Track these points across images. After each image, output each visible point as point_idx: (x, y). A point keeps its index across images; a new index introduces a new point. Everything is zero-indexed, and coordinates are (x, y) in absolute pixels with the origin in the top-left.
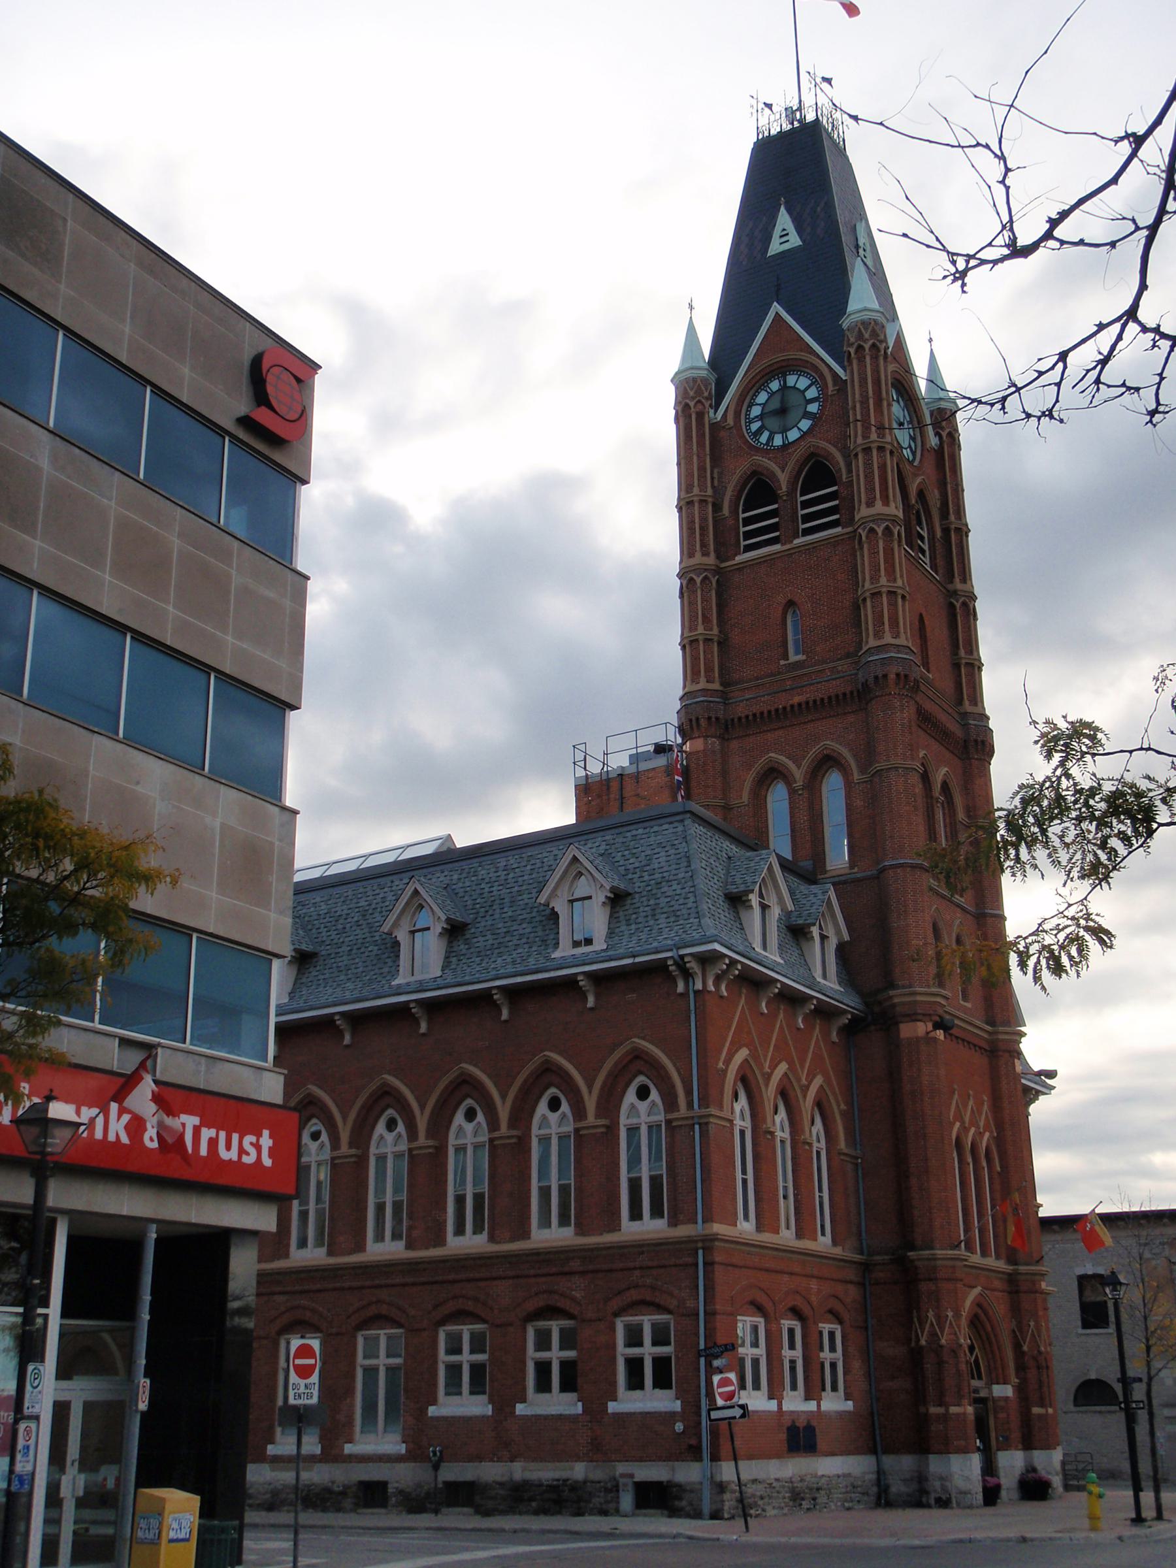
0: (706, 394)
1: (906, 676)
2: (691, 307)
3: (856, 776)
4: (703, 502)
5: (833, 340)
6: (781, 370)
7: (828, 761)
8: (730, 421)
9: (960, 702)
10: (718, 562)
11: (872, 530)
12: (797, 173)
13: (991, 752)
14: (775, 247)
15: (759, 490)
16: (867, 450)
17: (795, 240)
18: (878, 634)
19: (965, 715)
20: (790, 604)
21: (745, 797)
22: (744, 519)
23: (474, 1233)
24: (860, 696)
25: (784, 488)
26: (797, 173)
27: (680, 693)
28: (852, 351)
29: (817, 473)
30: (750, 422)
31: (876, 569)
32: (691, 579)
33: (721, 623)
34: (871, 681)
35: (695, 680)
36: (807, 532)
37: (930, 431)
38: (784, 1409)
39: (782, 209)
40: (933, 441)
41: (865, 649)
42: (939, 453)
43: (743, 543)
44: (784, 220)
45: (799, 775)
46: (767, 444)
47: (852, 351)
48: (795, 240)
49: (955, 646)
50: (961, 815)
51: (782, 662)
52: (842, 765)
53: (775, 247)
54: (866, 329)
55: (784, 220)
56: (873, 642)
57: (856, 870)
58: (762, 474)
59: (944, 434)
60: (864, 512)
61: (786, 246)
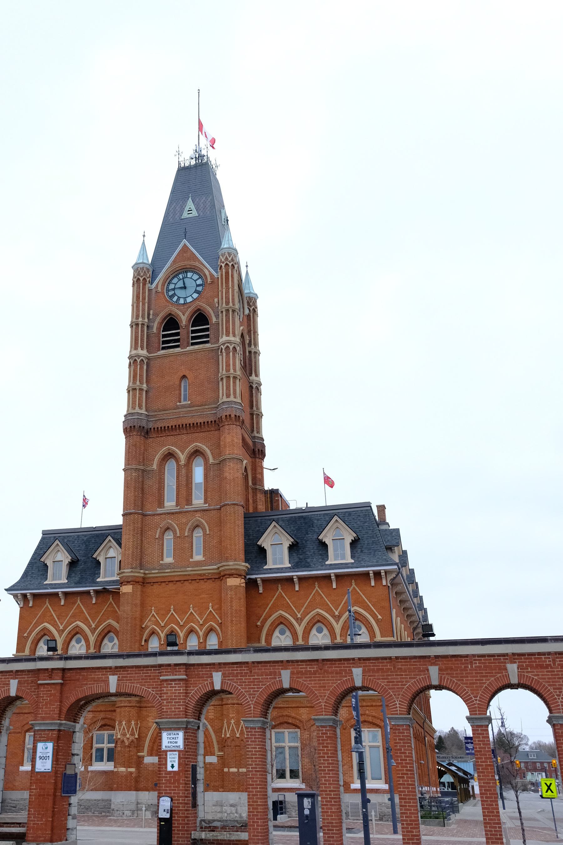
0: (148, 275)
1: (239, 417)
2: (144, 236)
3: (211, 460)
4: (143, 324)
5: (214, 260)
6: (185, 270)
7: (197, 453)
8: (159, 289)
9: (252, 431)
10: (147, 354)
11: (228, 347)
12: (195, 182)
13: (264, 456)
14: (185, 215)
15: (171, 323)
16: (227, 311)
17: (195, 213)
18: (228, 396)
19: (254, 437)
20: (184, 377)
21: (155, 467)
22: (163, 335)
23: (300, 626)
24: (217, 424)
25: (184, 323)
26: (195, 182)
27: (125, 413)
28: (223, 265)
29: (200, 318)
30: (169, 291)
31: (228, 365)
32: (135, 360)
33: (147, 382)
34: (224, 417)
35: (134, 408)
36: (193, 344)
37: (246, 306)
38: (206, 762)
39: (190, 198)
40: (247, 312)
41: (220, 402)
42: (249, 316)
43: (161, 346)
44: (190, 204)
45: (183, 457)
46: (176, 302)
47: (223, 265)
48: (195, 213)
49: (252, 407)
50: (250, 483)
51: (178, 404)
52: (175, 457)
53: (185, 215)
54: (230, 257)
55: (190, 204)
56: (225, 399)
57: (179, 507)
58: (173, 315)
59: (251, 309)
60: (224, 339)
61: (190, 215)
